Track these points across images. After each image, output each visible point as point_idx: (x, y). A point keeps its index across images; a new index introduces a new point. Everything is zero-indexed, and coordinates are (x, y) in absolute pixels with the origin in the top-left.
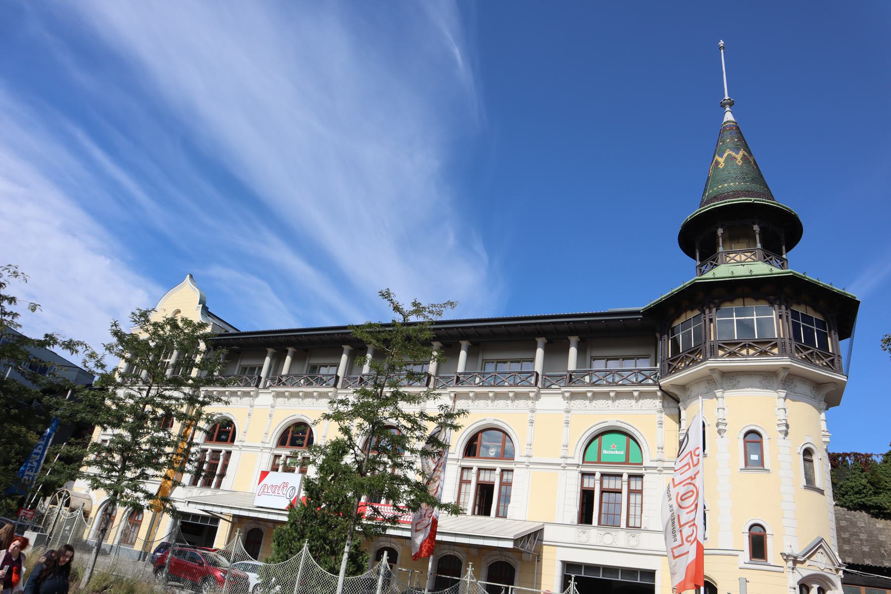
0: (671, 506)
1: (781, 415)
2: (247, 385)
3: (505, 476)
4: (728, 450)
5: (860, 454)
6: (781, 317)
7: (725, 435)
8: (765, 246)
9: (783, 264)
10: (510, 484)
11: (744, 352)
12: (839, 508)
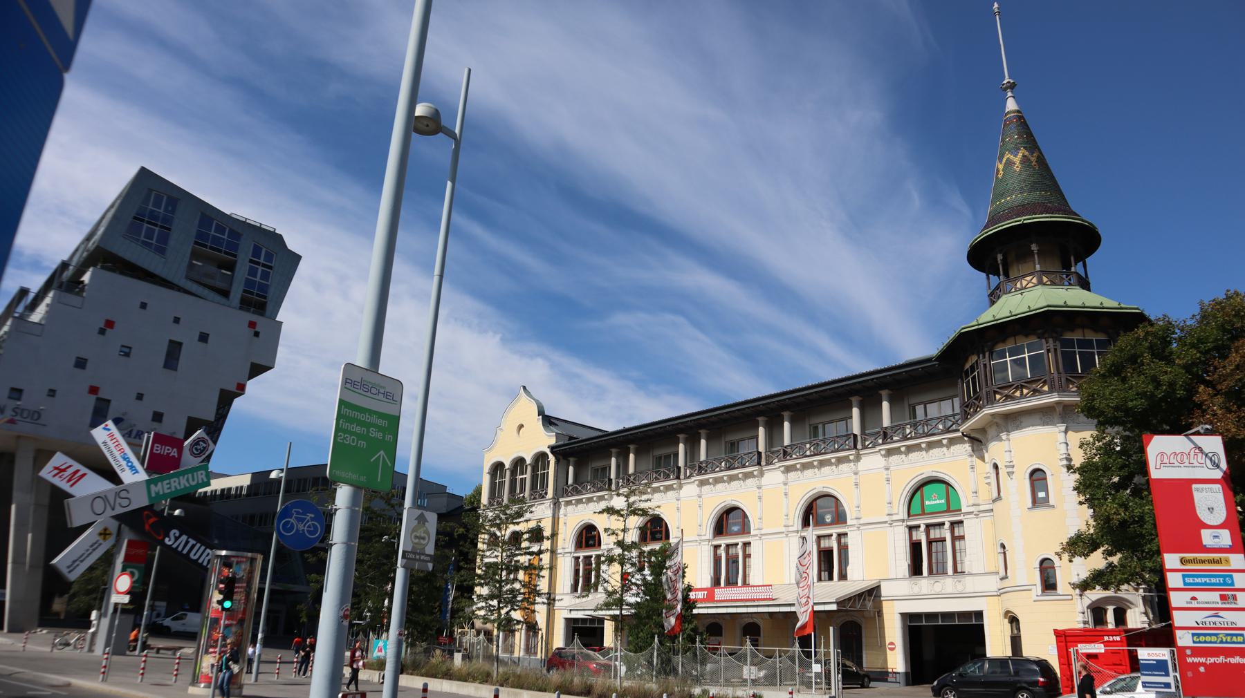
2: (667, 477)
4: (1017, 489)
10: (962, 538)
11: (1018, 394)
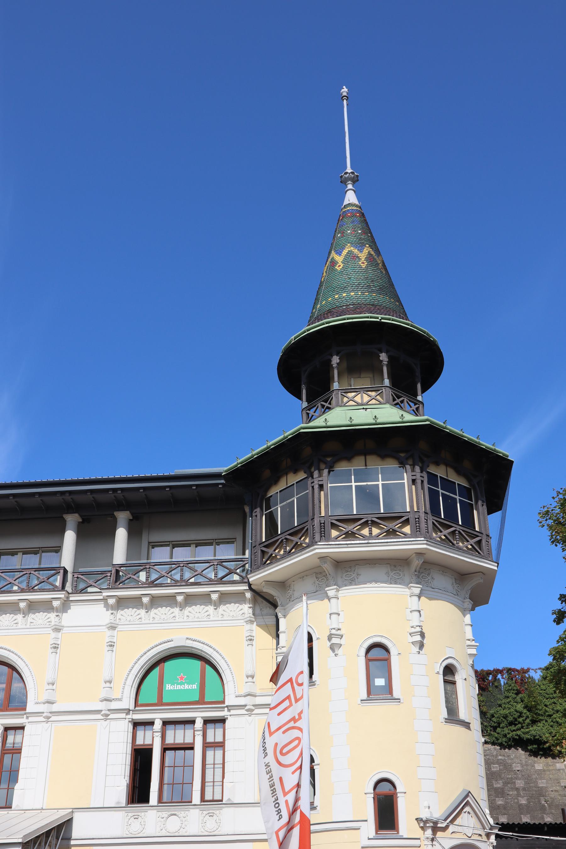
0: (267, 765)
1: (415, 619)
3: (10, 739)
4: (344, 671)
5: (514, 670)
6: (414, 481)
7: (340, 651)
8: (395, 384)
9: (417, 409)
11: (366, 532)
12: (489, 746)
